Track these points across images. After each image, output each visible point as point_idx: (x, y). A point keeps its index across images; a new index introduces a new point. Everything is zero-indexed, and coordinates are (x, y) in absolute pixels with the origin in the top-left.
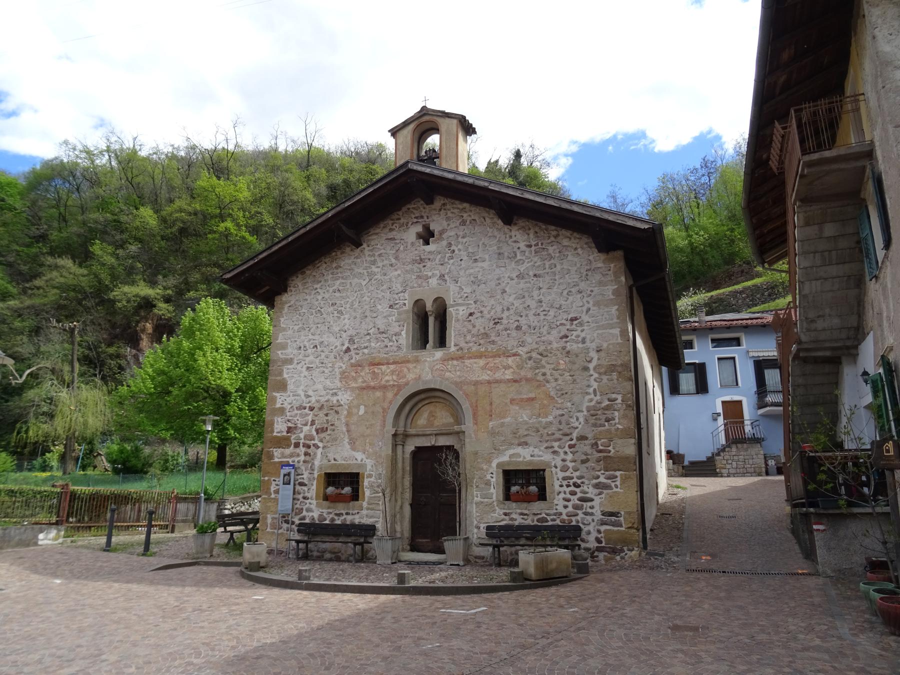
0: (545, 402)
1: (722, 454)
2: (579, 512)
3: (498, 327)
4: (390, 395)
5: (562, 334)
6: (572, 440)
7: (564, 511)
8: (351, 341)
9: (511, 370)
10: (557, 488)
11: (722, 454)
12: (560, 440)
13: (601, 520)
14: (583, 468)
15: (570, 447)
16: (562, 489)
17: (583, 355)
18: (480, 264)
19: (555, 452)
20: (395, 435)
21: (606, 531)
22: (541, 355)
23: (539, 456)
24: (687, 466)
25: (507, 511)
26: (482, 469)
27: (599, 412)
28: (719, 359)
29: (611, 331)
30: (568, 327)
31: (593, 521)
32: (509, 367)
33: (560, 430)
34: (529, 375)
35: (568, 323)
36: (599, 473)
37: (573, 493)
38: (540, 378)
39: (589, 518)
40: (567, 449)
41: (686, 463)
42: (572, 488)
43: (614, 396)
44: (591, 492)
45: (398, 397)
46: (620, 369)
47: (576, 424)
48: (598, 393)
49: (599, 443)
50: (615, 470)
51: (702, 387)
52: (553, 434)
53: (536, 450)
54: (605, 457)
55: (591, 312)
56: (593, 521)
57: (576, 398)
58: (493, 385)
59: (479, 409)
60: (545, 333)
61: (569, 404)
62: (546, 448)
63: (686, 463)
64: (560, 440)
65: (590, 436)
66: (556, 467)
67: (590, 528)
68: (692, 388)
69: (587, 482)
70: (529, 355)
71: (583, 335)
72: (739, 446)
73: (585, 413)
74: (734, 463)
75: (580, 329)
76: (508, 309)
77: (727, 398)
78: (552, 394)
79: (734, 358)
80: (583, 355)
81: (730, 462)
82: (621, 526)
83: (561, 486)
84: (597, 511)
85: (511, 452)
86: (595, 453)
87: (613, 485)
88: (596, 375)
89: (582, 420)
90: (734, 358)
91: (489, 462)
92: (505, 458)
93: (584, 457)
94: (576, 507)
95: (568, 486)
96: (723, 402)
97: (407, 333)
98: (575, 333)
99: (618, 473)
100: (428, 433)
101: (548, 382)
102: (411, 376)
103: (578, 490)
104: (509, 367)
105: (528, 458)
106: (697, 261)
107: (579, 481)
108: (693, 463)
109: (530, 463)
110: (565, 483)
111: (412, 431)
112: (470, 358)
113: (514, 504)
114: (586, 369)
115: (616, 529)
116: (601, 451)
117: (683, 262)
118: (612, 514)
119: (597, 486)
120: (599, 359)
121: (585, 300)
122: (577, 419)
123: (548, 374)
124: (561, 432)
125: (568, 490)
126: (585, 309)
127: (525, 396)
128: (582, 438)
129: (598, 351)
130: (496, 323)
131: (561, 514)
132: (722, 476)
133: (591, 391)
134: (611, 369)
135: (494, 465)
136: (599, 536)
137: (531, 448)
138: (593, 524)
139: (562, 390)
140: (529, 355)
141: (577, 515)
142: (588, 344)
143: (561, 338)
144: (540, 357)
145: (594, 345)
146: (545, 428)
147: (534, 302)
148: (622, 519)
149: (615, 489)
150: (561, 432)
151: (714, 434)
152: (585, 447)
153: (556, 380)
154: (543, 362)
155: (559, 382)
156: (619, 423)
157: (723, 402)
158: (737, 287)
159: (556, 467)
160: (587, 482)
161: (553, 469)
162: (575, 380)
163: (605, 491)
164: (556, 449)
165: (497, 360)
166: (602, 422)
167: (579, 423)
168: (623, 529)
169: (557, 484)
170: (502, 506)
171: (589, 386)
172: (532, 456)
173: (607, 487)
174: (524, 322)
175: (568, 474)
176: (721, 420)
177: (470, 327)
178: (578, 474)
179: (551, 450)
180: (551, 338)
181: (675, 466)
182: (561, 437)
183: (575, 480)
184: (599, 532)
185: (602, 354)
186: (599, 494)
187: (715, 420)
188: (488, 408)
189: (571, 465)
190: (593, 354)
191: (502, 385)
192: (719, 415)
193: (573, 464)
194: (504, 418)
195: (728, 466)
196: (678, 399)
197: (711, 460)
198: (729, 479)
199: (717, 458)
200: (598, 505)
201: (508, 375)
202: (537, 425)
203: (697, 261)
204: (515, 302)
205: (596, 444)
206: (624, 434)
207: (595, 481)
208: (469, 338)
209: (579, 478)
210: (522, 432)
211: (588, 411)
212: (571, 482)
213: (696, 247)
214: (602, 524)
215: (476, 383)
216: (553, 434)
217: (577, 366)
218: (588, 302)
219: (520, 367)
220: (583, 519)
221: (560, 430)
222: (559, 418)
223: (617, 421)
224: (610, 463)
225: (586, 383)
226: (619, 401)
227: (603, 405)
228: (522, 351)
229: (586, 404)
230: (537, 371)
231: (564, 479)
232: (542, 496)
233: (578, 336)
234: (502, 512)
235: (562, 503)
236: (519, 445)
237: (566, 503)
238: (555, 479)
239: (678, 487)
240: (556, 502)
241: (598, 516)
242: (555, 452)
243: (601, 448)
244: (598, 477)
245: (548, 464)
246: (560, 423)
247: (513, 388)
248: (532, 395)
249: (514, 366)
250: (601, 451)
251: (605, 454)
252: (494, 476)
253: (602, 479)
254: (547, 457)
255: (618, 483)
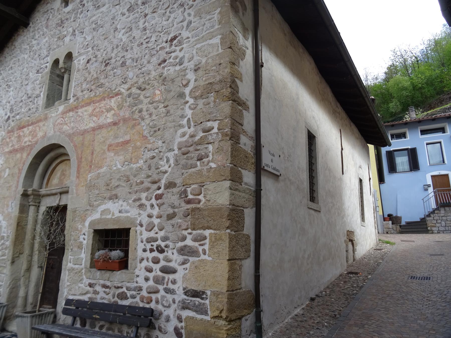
0: (138, 144)
1: (432, 215)
2: (161, 287)
3: (109, 68)
4: (25, 155)
5: (161, 59)
6: (159, 188)
7: (145, 285)
8: (12, 110)
9: (113, 112)
10: (140, 253)
11: (432, 215)
12: (148, 189)
13: (183, 302)
14: (168, 225)
15: (158, 197)
16: (145, 255)
17: (179, 79)
18: (102, 9)
19: (141, 206)
20: (25, 195)
21: (189, 318)
22: (140, 88)
23: (127, 212)
24: (404, 226)
25: (92, 282)
26: (77, 229)
27: (191, 149)
28: (427, 144)
29: (211, 42)
30: (168, 50)
31: (174, 302)
32: (111, 109)
33: (149, 176)
34: (127, 115)
35: (168, 45)
36: (185, 233)
37: (156, 261)
38: (136, 116)
39: (170, 297)
40: (153, 201)
41: (403, 223)
42: (155, 254)
43: (209, 124)
44: (176, 259)
45: (30, 157)
46: (217, 87)
47: (166, 168)
48: (192, 124)
49: (189, 190)
50: (204, 228)
51: (414, 165)
52: (142, 183)
53: (125, 204)
54: (193, 210)
55: (193, 24)
56: (174, 302)
57: (167, 135)
58: (97, 132)
59: (83, 160)
60: (146, 62)
61: (160, 142)
62: (134, 201)
63: (403, 223)
64: (148, 189)
65: (178, 181)
66: (141, 225)
67: (170, 312)
68: (407, 167)
69: (171, 245)
70: (129, 92)
71: (181, 55)
72: (447, 209)
73: (176, 152)
74: (443, 223)
75: (178, 48)
76: (117, 46)
77: (436, 173)
78: (145, 133)
79: (440, 143)
80: (179, 79)
81: (439, 221)
82: (206, 313)
83: (145, 250)
84: (179, 288)
85: (103, 207)
86: (183, 204)
87: (200, 249)
88: (191, 101)
89: (172, 161)
90: (440, 143)
91: (84, 221)
92: (96, 216)
93: (171, 211)
94: (157, 280)
95: (152, 251)
96: (432, 176)
97: (44, 94)
98: (173, 55)
99: (207, 233)
100: (54, 192)
101: (143, 119)
102: (40, 134)
103: (161, 256)
104: (111, 109)
105: (117, 214)
106: (418, 94)
107: (163, 244)
108: (409, 224)
109: (118, 220)
110: (148, 246)
111: (43, 191)
112: (82, 107)
113: (98, 273)
114: (181, 95)
115: (199, 317)
116: (189, 202)
117: (407, 96)
118: (196, 294)
119: (182, 251)
120: (196, 80)
121: (186, 14)
122: (168, 161)
123: (144, 109)
124: (149, 180)
125: (151, 256)
126: (185, 24)
127: (121, 140)
128: (170, 185)
129: (196, 70)
130: (106, 65)
131: (140, 289)
132: (433, 233)
133: (191, 121)
134: (209, 88)
135: (87, 224)
136: (180, 325)
137: (121, 202)
138: (174, 306)
139: (155, 126)
140: (129, 92)
141: (157, 292)
142: (186, 64)
143: (160, 64)
144: (139, 92)
145: (191, 65)
146: (135, 176)
147: (139, 31)
148: (207, 302)
149: (203, 257)
150: (149, 180)
151: (425, 201)
152: (172, 197)
153: (151, 115)
154: (142, 97)
155: (154, 117)
156: (212, 161)
157: (432, 176)
158: (446, 106)
159: (141, 225)
160: (171, 245)
161: (139, 228)
162: (168, 112)
163: (191, 259)
164: (144, 201)
165: (103, 104)
166: (193, 161)
167: (168, 167)
168: (208, 318)
169: (141, 246)
170: (89, 274)
171: (182, 117)
172: (120, 212)
173: (193, 252)
174: (129, 56)
175: (152, 234)
176: (431, 189)
177: (87, 75)
178: (162, 234)
179: (138, 203)
180: (150, 67)
181: (394, 226)
182: (149, 185)
183: (159, 242)
184: (180, 319)
185: (200, 72)
186: (183, 263)
187: (426, 190)
188: (90, 158)
189: (156, 221)
190: (191, 76)
191: (104, 131)
192: (429, 186)
193: (159, 220)
194: (101, 167)
195: (438, 225)
196: (395, 176)
197: (423, 221)
198: (439, 235)
199: (428, 218)
200: (181, 280)
201: (109, 118)
202: (128, 173)
203: (418, 94)
204: (123, 37)
205: (185, 192)
206: (217, 176)
207: (181, 244)
208: (84, 86)
209: (165, 239)
210: (115, 183)
211: (179, 149)
212: (155, 244)
213: (417, 85)
214: (184, 308)
215: (84, 133)
216: (142, 183)
217: (172, 94)
218: (189, 15)
219: (120, 107)
220: (163, 297)
221: (149, 176)
222: (149, 161)
223: (210, 158)
224: (197, 217)
225: (179, 112)
226: (215, 130)
227: (197, 138)
228: (123, 89)
229: (178, 140)
230: (135, 108)
231: (149, 240)
232: (123, 264)
233: (176, 57)
234: (87, 281)
235: (143, 273)
236: (110, 199)
237: (148, 274)
238: (139, 241)
239: (387, 243)
240: (137, 272)
241: (180, 296)
242: (141, 206)
243: (190, 197)
244: (184, 239)
245: (132, 221)
246: (150, 167)
247: (112, 133)
248: (127, 138)
249: (115, 108)
250: (189, 202)
251: (193, 206)
252: (86, 237)
253: (189, 242)
254: (133, 213)
255: (206, 247)
